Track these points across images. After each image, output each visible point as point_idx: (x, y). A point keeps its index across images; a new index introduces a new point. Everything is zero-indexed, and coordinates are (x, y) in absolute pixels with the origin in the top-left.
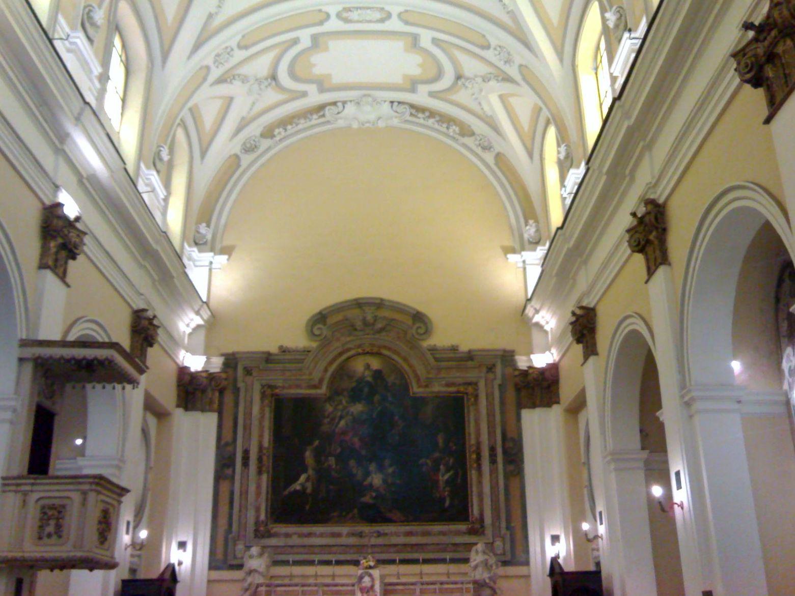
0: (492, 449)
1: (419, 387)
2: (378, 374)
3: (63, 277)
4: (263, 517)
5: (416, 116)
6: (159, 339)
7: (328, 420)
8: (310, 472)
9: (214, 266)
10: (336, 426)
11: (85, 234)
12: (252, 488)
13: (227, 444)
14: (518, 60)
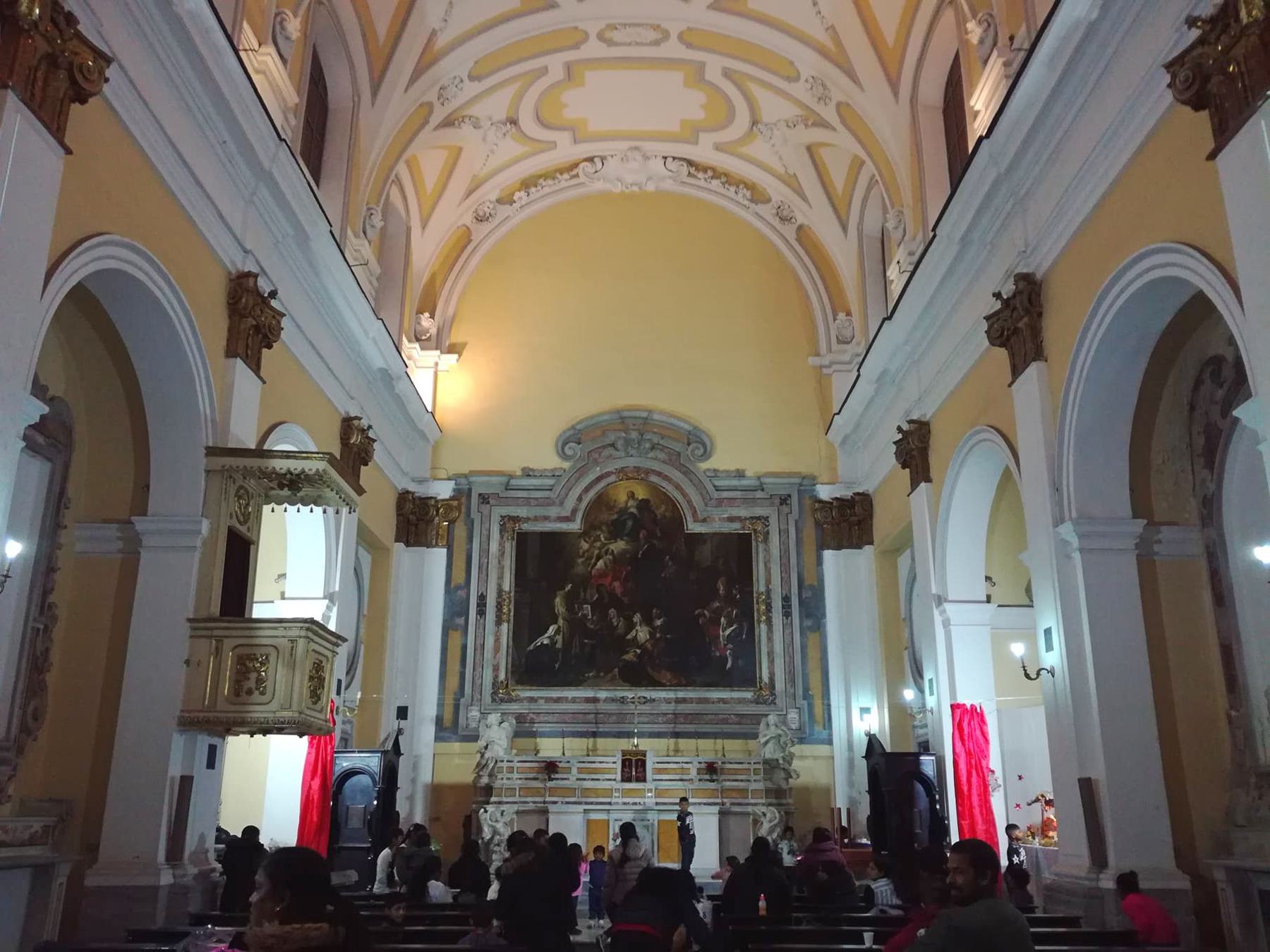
0: (786, 599)
1: (696, 521)
2: (644, 505)
3: (255, 366)
4: (502, 676)
5: (695, 177)
6: (375, 457)
7: (583, 559)
8: (561, 622)
9: (440, 368)
10: (593, 567)
11: (283, 315)
12: (490, 641)
13: (458, 588)
14: (837, 96)
